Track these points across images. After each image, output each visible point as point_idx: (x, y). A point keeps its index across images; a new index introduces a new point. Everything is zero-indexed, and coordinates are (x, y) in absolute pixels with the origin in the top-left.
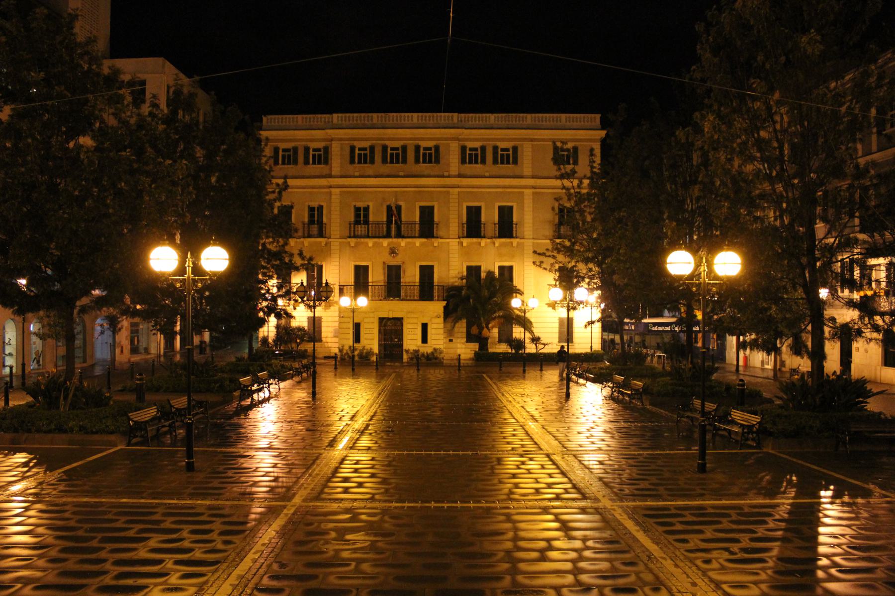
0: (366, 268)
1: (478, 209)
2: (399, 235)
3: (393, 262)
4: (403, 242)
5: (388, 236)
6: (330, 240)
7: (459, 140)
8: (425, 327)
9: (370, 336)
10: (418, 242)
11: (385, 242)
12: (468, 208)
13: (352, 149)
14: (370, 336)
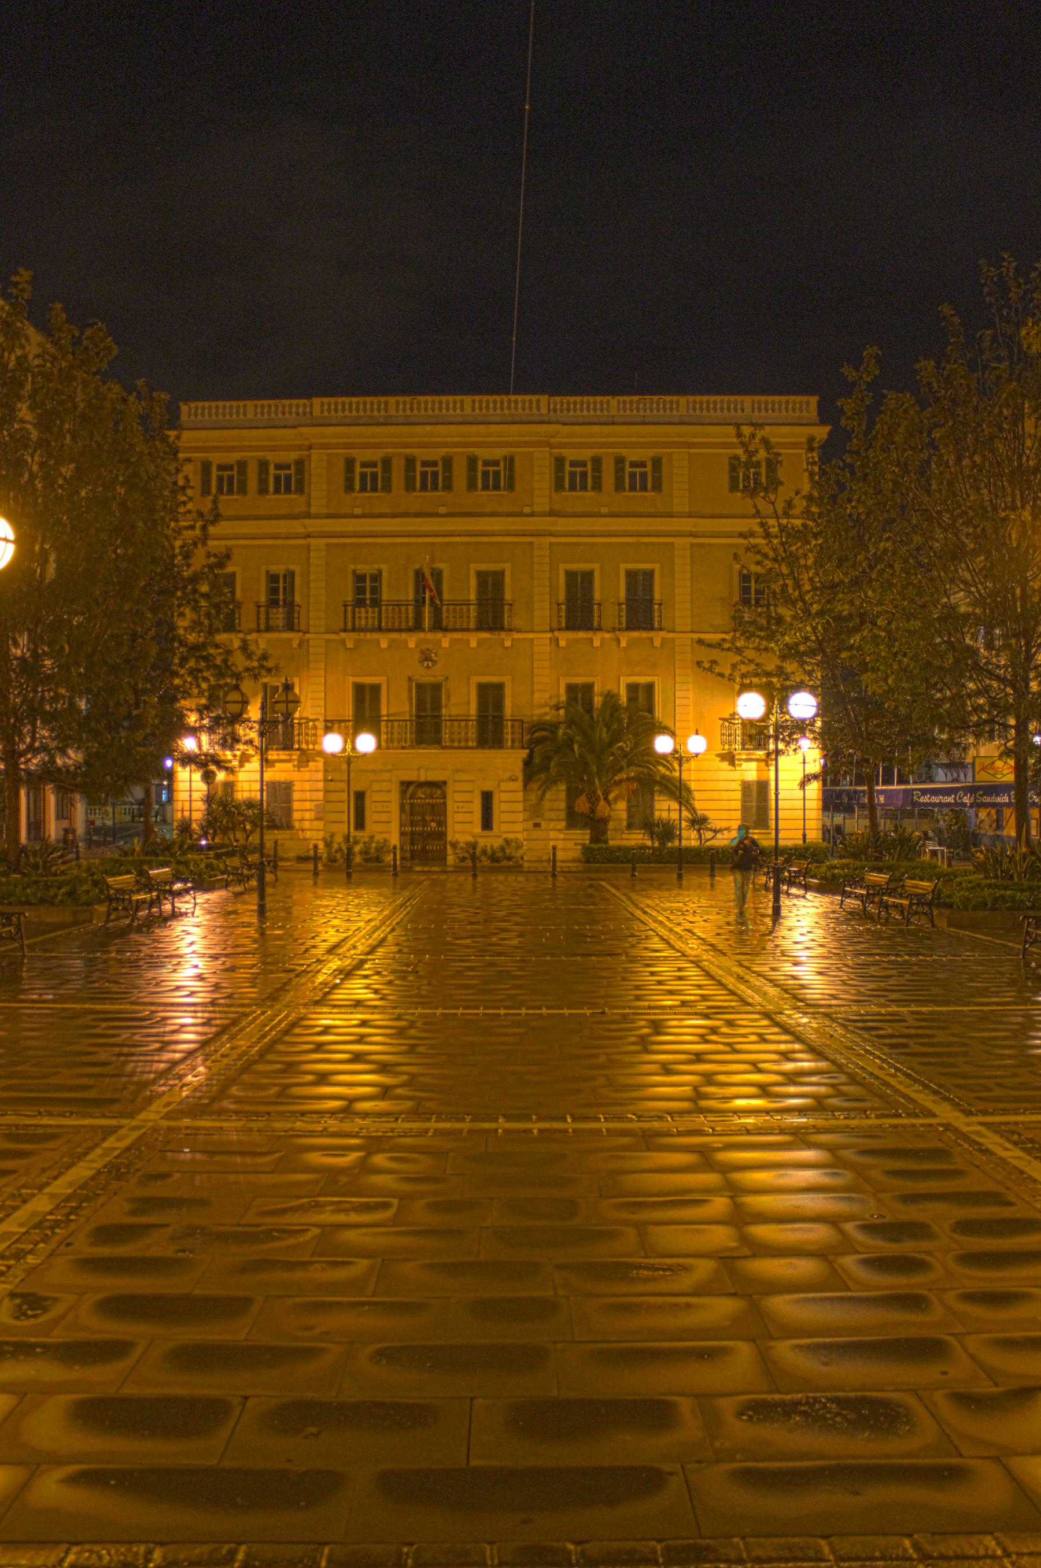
0: (376, 689)
1: (588, 577)
2: (438, 626)
3: (428, 677)
4: (446, 640)
5: (418, 626)
6: (308, 636)
7: (550, 445)
8: (487, 798)
9: (383, 817)
10: (473, 639)
11: (412, 641)
12: (480, 574)
13: (350, 463)
14: (383, 817)
